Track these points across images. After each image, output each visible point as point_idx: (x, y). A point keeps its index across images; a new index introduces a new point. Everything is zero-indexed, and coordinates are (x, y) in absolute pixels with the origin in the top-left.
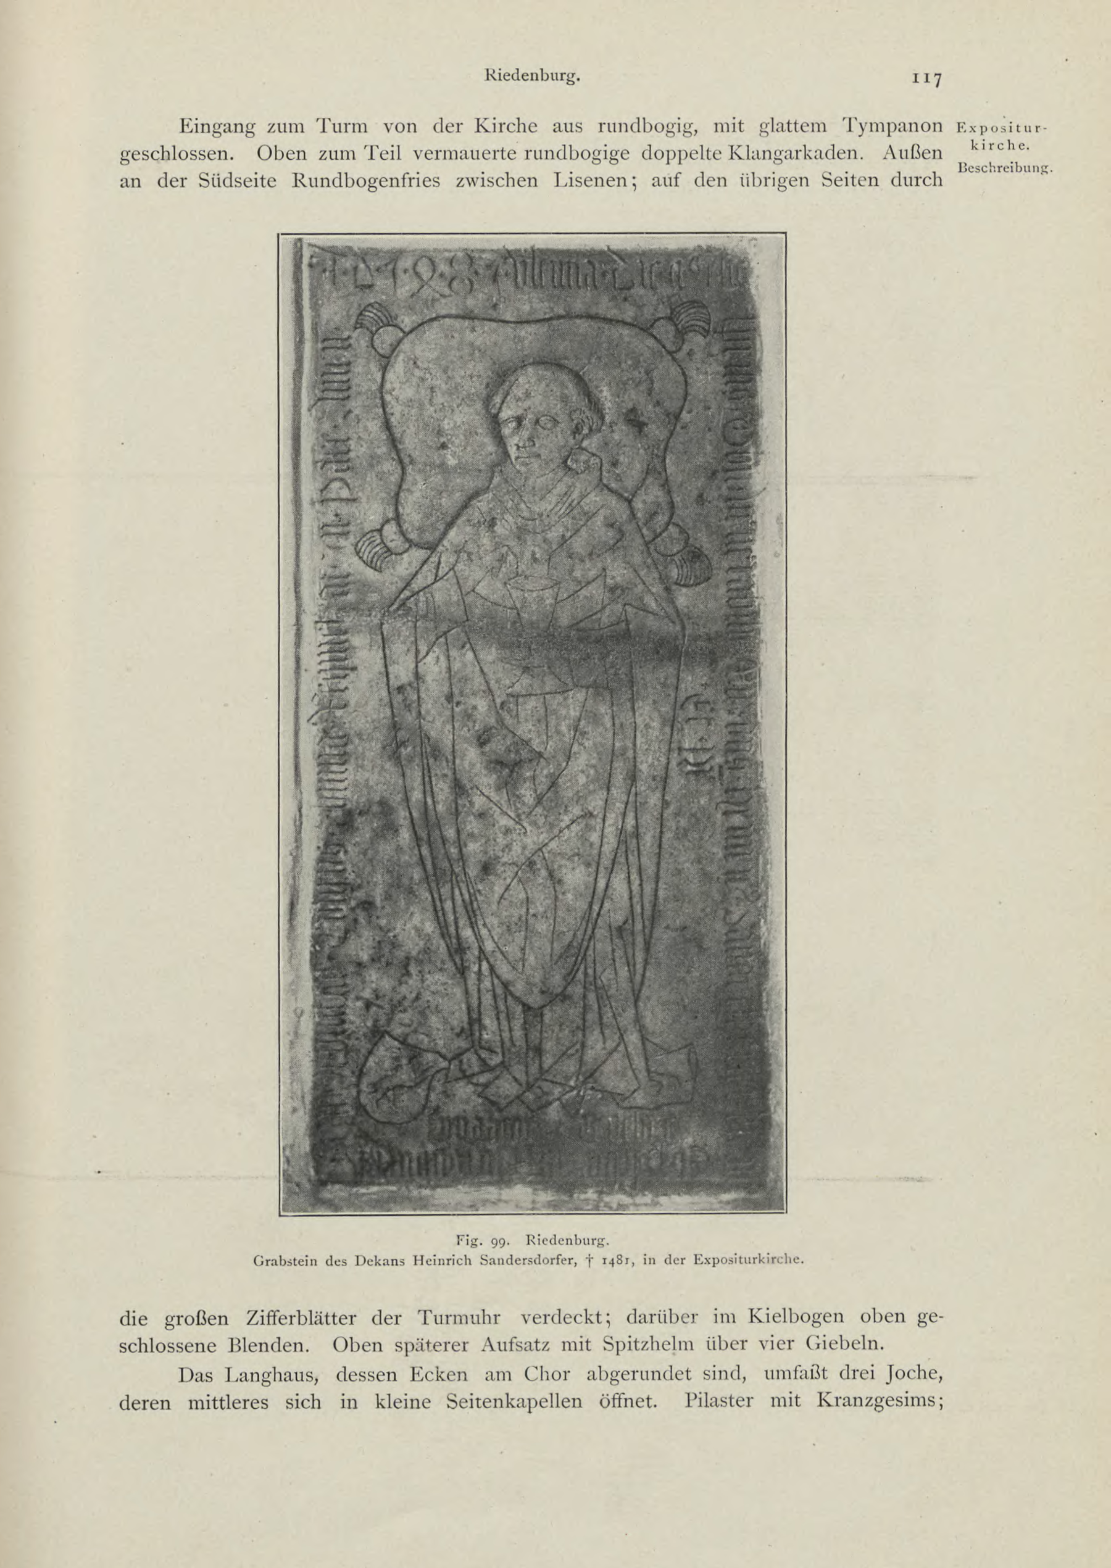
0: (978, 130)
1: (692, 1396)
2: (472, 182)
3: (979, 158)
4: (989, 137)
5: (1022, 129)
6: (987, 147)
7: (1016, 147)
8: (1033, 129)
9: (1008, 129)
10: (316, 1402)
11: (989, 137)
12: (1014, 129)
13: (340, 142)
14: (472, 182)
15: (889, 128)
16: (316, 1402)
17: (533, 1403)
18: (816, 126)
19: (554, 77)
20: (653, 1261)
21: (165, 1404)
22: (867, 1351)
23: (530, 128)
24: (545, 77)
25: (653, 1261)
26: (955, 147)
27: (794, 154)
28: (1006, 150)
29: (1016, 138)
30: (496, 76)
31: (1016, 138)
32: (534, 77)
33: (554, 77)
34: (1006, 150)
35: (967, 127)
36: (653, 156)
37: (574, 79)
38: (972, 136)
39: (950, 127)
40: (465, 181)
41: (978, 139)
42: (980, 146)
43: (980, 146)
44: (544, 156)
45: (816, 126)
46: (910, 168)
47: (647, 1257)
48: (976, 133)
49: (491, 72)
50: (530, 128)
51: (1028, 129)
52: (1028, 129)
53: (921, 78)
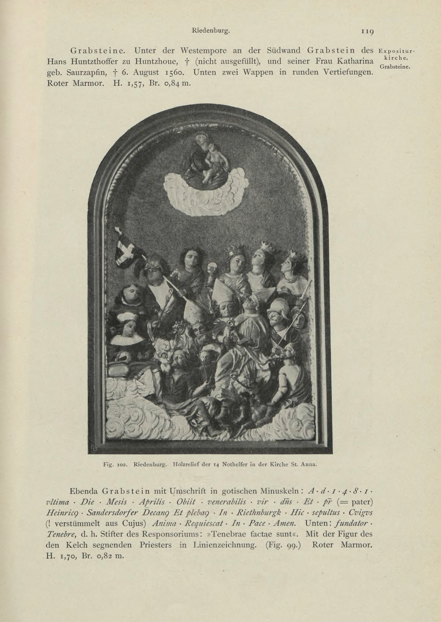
0: (387, 52)
1: (143, 543)
2: (229, 73)
3: (387, 63)
4: (392, 55)
5: (405, 51)
6: (391, 58)
7: (402, 59)
8: (409, 52)
9: (399, 52)
10: (85, 545)
11: (392, 55)
12: (402, 51)
13: (276, 57)
14: (229, 73)
15: (198, 51)
16: (85, 545)
17: (158, 535)
18: (205, 51)
19: (220, 31)
20: (254, 465)
21: (57, 546)
22: (294, 494)
23: (224, 51)
24: (216, 31)
25: (254, 465)
26: (378, 58)
27: (359, 62)
28: (396, 60)
29: (402, 55)
30: (197, 31)
31: (402, 55)
32: (211, 31)
33: (220, 31)
34: (396, 60)
35: (383, 51)
36: (205, 63)
37: (228, 32)
38: (385, 54)
39: (376, 51)
40: (226, 73)
41: (387, 56)
42: (388, 58)
43: (388, 58)
44: (83, 63)
45: (205, 51)
46: (203, 67)
47: (252, 464)
48: (387, 53)
49: (194, 29)
50: (224, 51)
51: (407, 52)
52: (407, 52)
53: (365, 31)
